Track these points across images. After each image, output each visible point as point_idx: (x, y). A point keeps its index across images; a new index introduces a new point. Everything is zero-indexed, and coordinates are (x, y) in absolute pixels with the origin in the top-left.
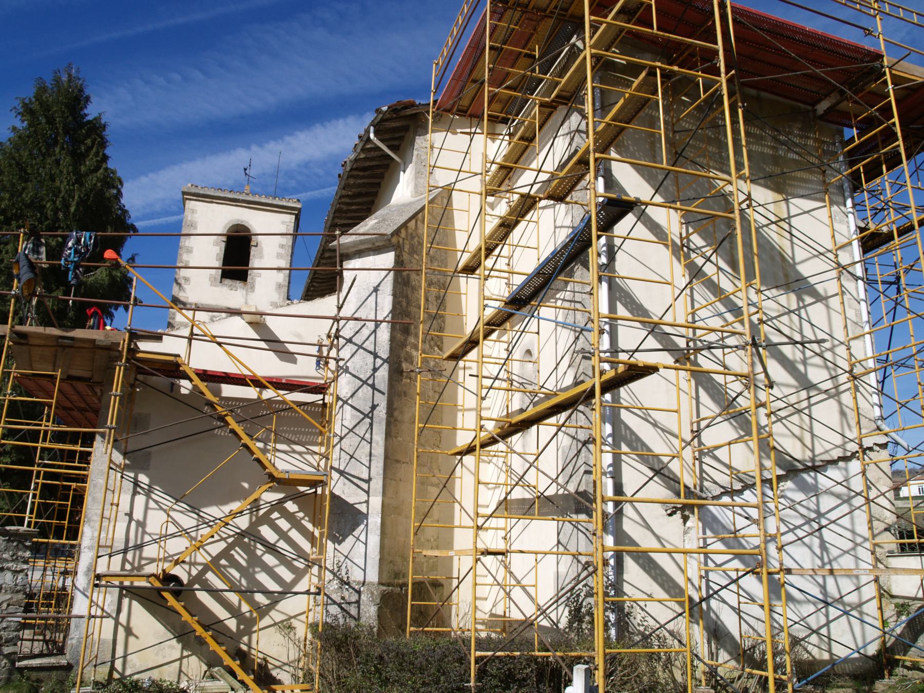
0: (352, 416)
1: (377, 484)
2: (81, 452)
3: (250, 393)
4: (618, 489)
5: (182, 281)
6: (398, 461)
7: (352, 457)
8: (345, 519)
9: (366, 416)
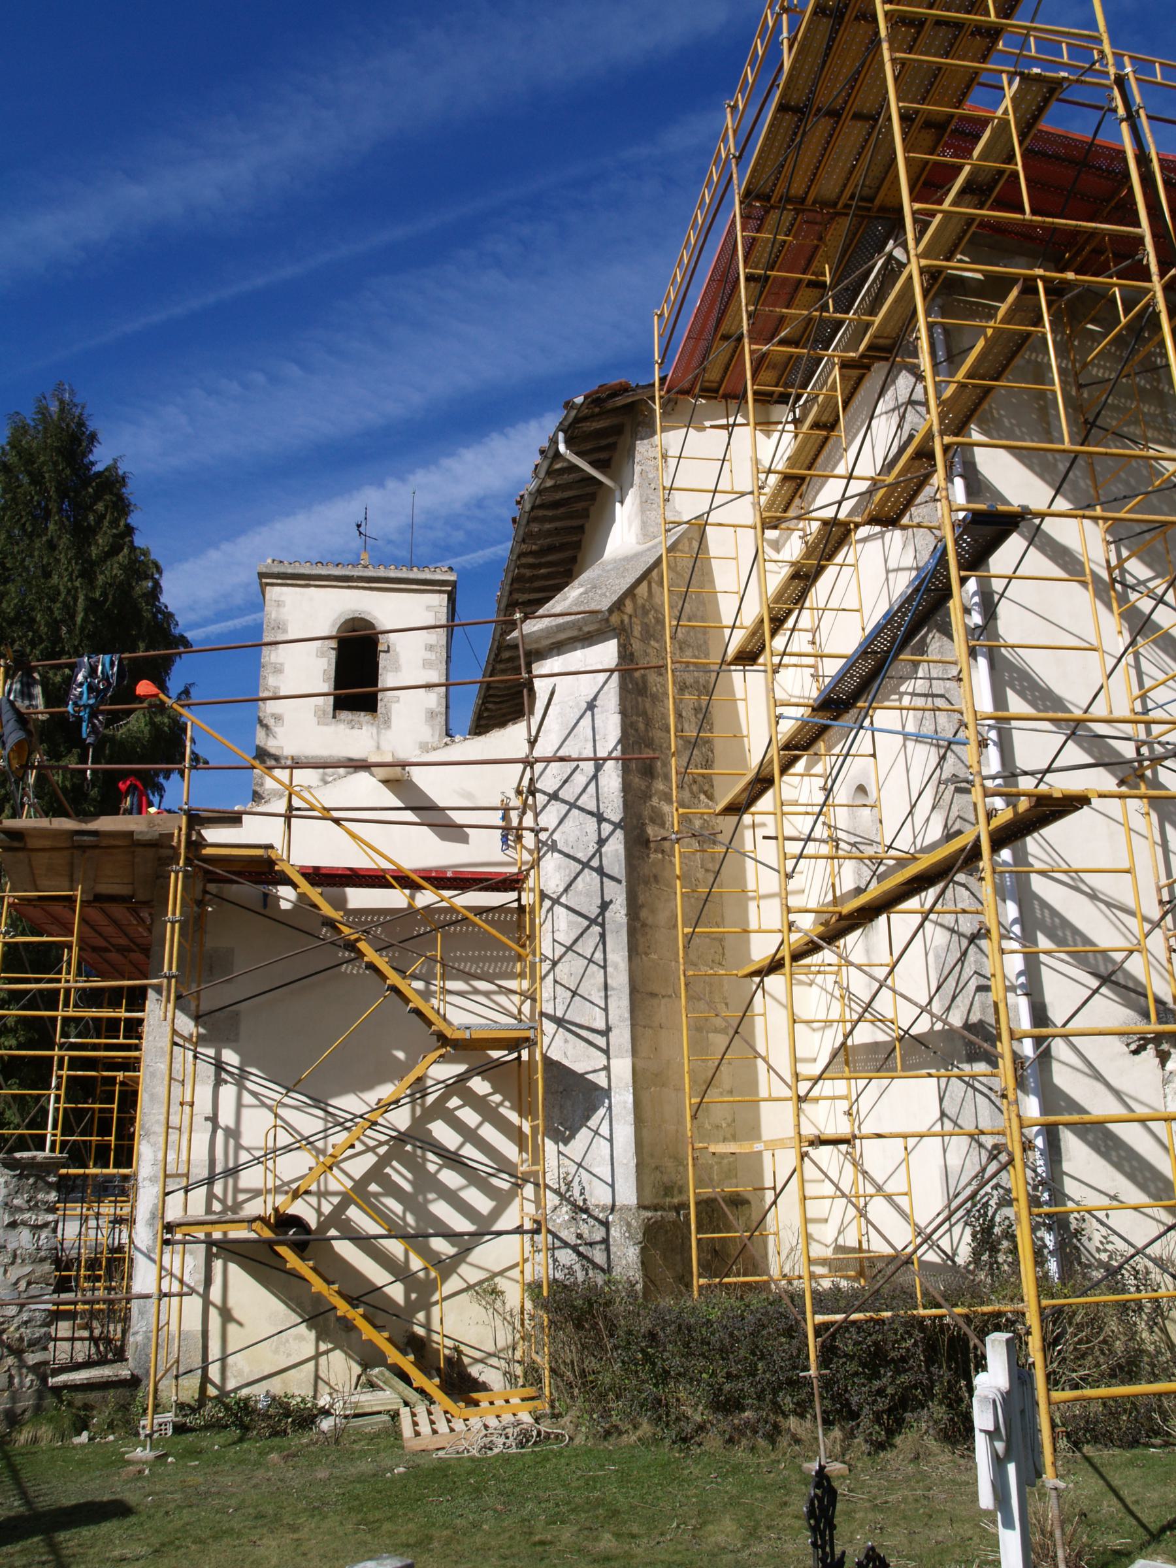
0: (570, 924)
1: (621, 1037)
2: (127, 1020)
3: (396, 898)
4: (1040, 1015)
5: (270, 722)
6: (653, 995)
7: (574, 993)
8: (571, 1101)
9: (593, 922)
